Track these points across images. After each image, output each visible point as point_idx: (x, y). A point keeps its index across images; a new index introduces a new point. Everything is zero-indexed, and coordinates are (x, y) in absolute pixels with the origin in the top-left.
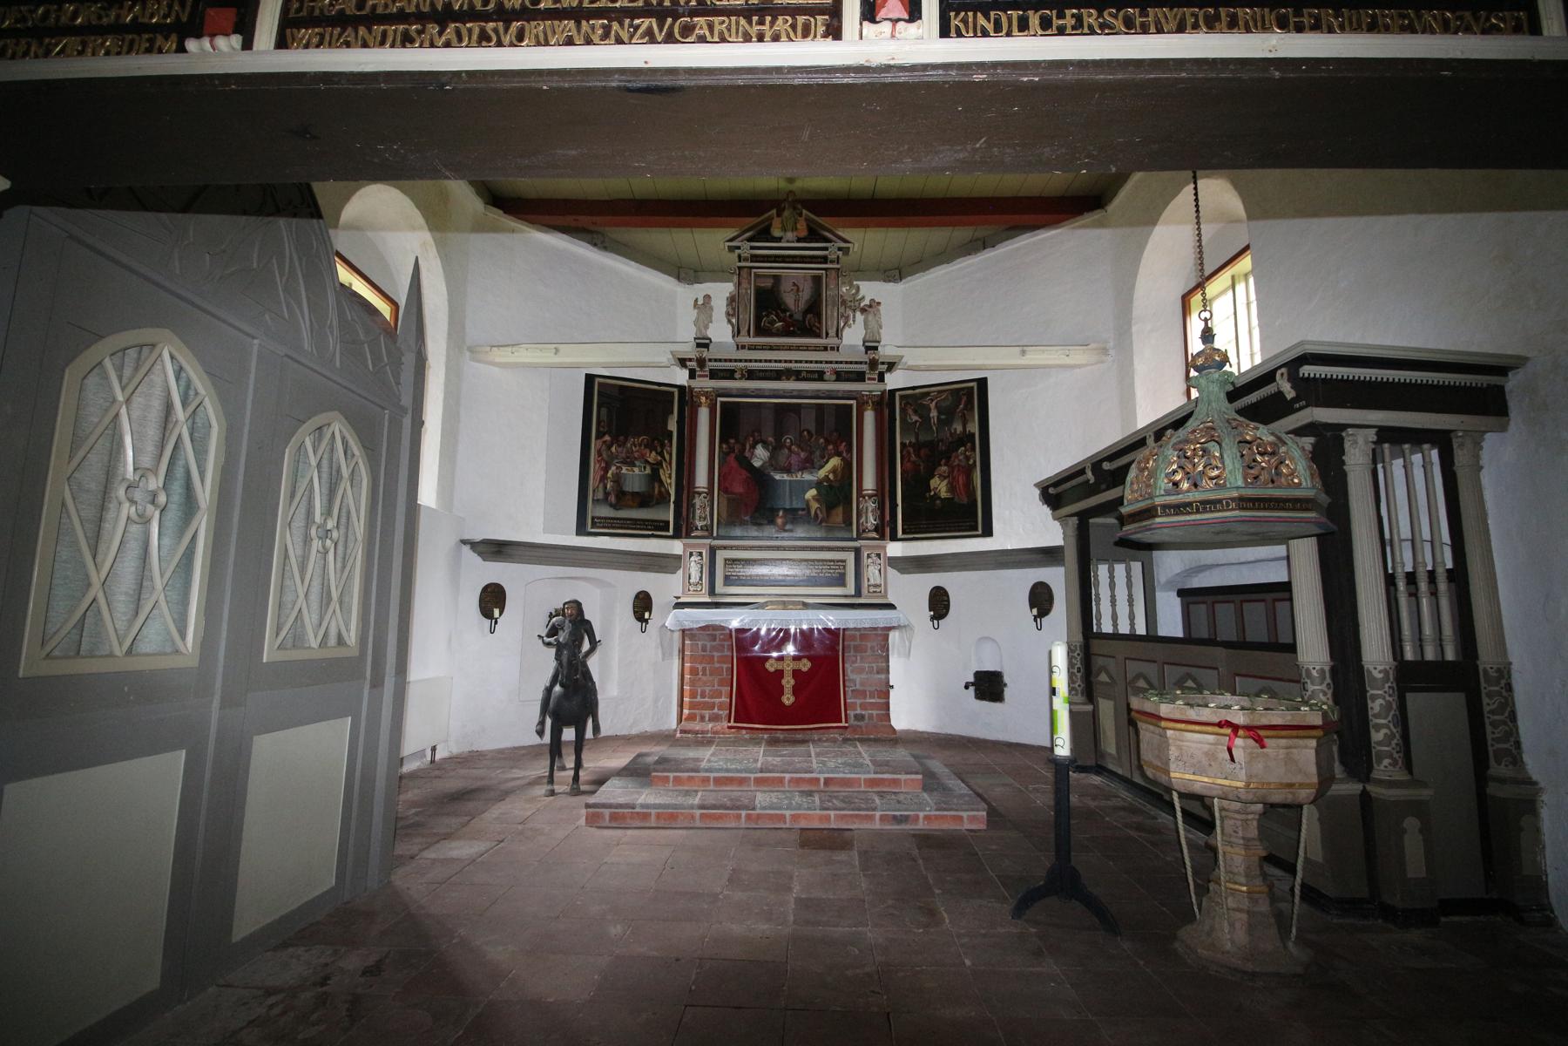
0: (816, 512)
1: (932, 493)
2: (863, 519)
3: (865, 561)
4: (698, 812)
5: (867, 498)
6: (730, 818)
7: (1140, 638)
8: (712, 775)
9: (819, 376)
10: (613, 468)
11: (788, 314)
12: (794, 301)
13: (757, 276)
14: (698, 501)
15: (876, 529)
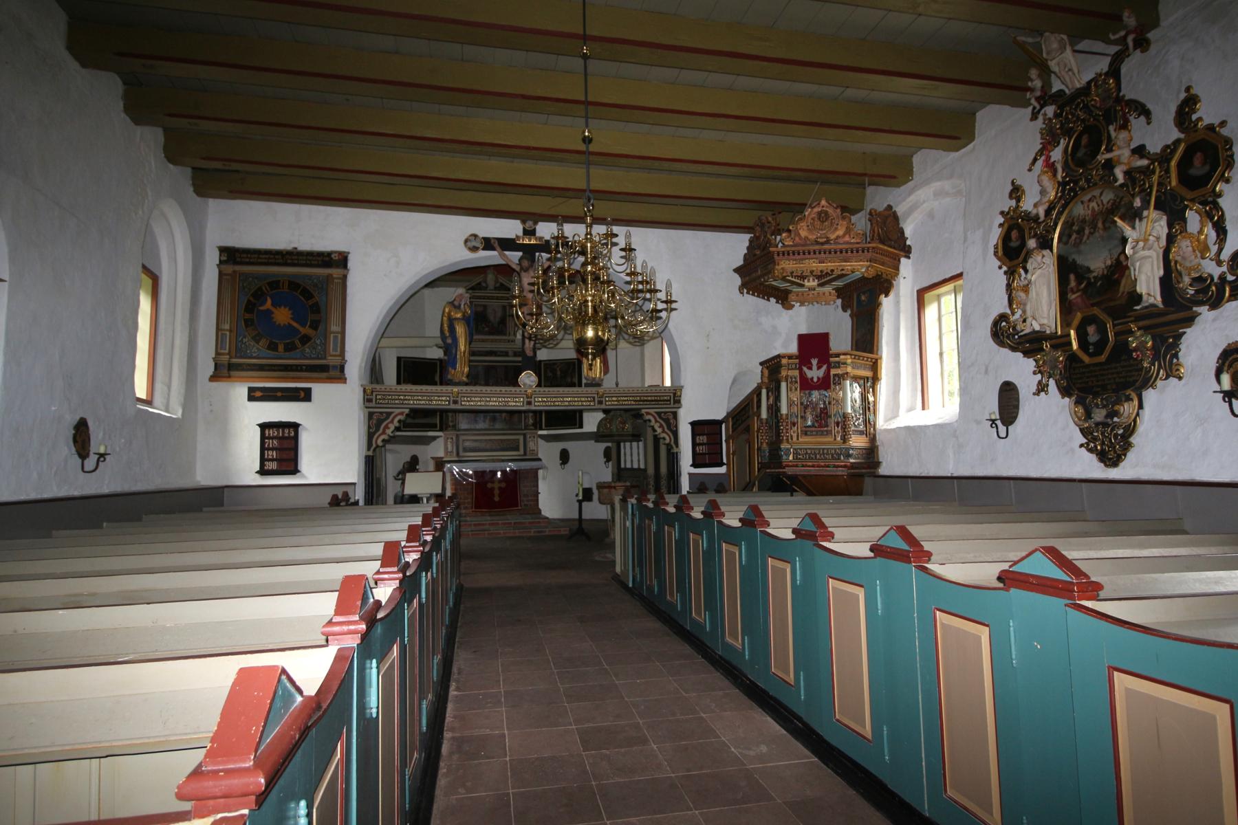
2: (527, 420)
3: (528, 439)
4: (470, 533)
6: (584, 281)
7: (628, 469)
8: (473, 523)
9: (506, 354)
12: (494, 317)
13: (475, 305)
15: (533, 425)
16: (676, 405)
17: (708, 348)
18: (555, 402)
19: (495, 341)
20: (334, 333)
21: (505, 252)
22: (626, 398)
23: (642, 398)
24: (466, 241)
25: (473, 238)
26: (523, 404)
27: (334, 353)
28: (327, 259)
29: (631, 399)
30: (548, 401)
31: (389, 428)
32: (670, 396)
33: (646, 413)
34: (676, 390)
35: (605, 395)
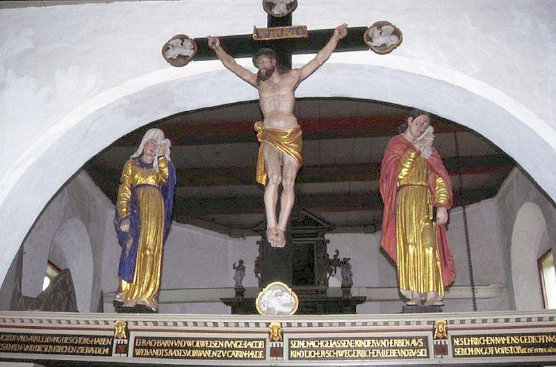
21: (236, 60)
22: (503, 340)
23: (542, 339)
24: (166, 49)
26: (264, 354)
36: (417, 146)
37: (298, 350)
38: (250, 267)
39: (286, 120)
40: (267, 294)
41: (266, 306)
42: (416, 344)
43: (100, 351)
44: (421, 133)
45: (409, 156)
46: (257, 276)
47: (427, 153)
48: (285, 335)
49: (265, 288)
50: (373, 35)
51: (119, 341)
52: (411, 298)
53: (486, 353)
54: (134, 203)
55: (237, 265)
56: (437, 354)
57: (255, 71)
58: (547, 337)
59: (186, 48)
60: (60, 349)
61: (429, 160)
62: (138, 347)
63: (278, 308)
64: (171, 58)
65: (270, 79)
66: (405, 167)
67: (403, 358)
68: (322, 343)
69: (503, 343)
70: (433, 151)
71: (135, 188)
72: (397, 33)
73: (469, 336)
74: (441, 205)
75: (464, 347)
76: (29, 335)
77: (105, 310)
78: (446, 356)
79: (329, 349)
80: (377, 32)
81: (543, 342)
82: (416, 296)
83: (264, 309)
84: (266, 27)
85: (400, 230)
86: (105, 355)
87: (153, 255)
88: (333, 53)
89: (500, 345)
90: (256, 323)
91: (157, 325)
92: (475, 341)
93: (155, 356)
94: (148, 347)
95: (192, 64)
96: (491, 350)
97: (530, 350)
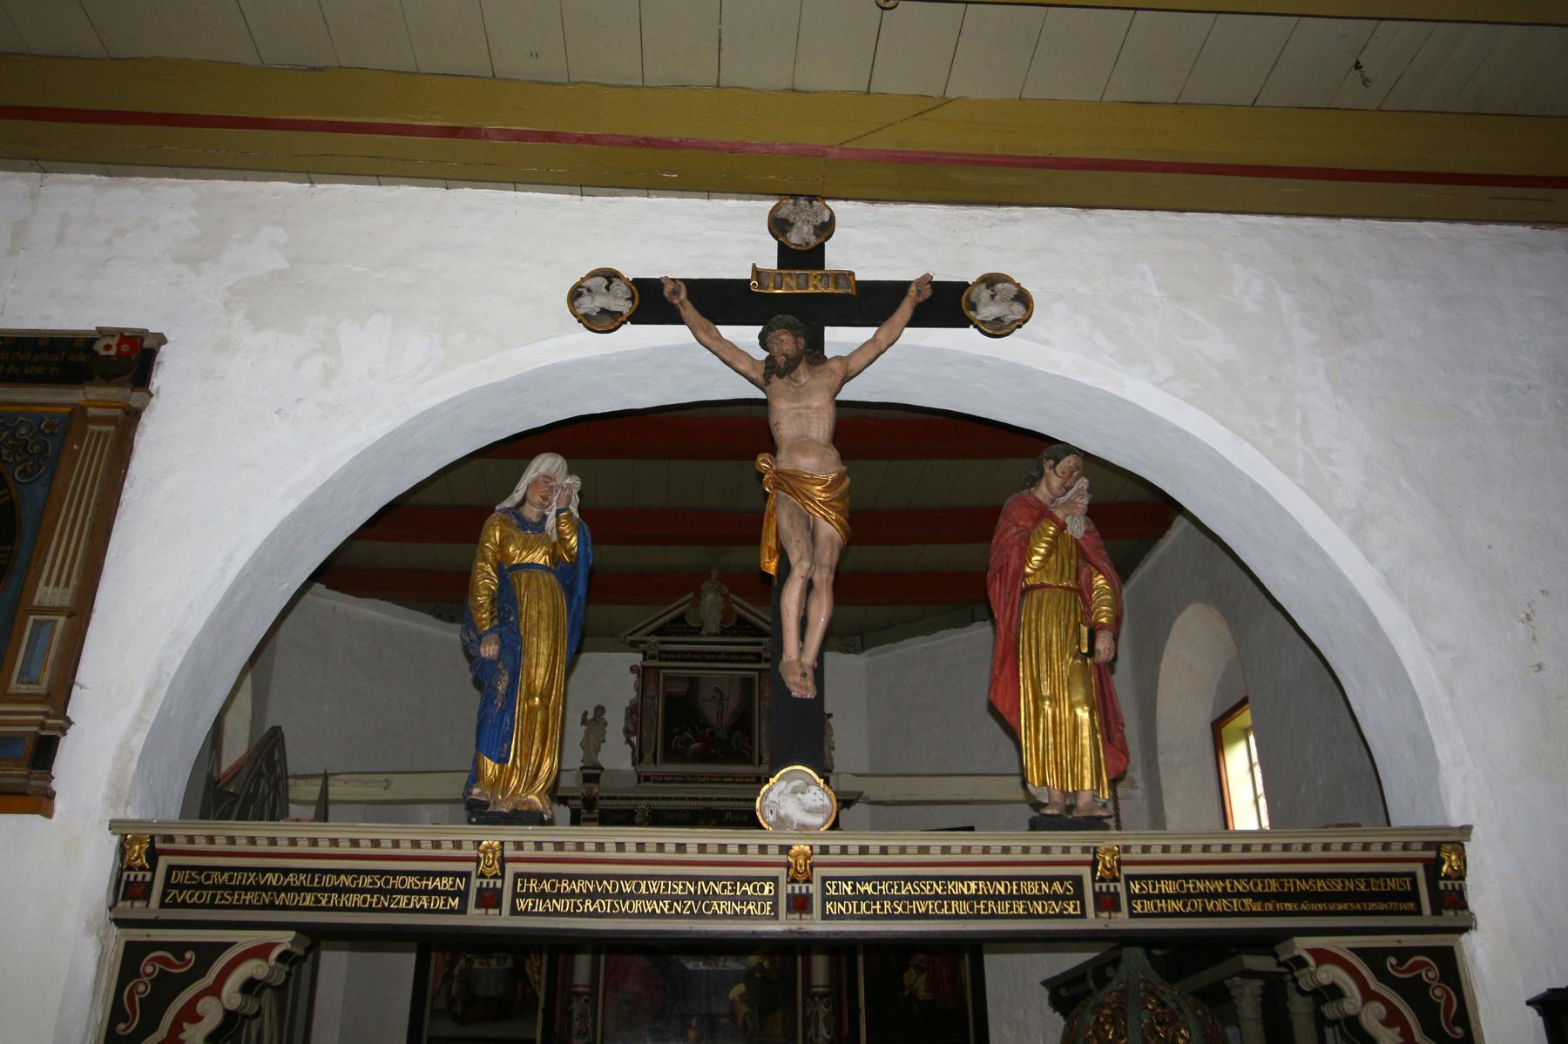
0: (744, 1021)
1: (907, 993)
2: (811, 1033)
5: (817, 999)
10: (462, 962)
11: (708, 730)
13: (667, 678)
14: (576, 1008)
16: (1449, 917)
17: (1540, 667)
18: (911, 898)
19: (721, 779)
20: (43, 610)
21: (720, 328)
22: (1219, 885)
23: (1289, 885)
24: (575, 294)
25: (602, 281)
26: (775, 907)
27: (24, 689)
28: (83, 358)
29: (1239, 886)
30: (882, 897)
31: (196, 1018)
32: (1413, 875)
33: (1312, 951)
34: (1437, 846)
35: (1126, 870)
36: (1059, 514)
37: (841, 899)
38: (616, 722)
39: (823, 456)
40: (776, 790)
41: (775, 812)
42: (1060, 891)
43: (440, 904)
44: (1068, 489)
45: (1045, 530)
46: (628, 741)
47: (1077, 527)
48: (815, 870)
49: (773, 777)
50: (979, 300)
51: (133, 874)
52: (1047, 801)
53: (1189, 909)
54: (506, 601)
55: (590, 716)
56: (1102, 911)
57: (761, 355)
58: (1298, 882)
59: (615, 297)
60: (357, 899)
61: (1082, 542)
62: (521, 896)
63: (799, 816)
64: (585, 315)
65: (792, 375)
66: (1037, 553)
67: (1039, 916)
68: (885, 886)
69: (1220, 890)
70: (1088, 524)
71: (506, 572)
72: (1023, 298)
73: (1159, 877)
74: (1103, 626)
75: (1149, 897)
76: (286, 872)
77: (330, 818)
78: (808, 917)
79: (900, 898)
80: (985, 294)
81: (1292, 890)
82: (1057, 796)
83: (771, 818)
84: (775, 266)
85: (1028, 672)
86: (452, 911)
87: (547, 707)
88: (906, 329)
89: (1214, 895)
90: (535, 843)
91: (562, 849)
92: (1169, 887)
93: (556, 913)
94: (543, 896)
95: (628, 328)
96: (1198, 903)
97: (1269, 906)
